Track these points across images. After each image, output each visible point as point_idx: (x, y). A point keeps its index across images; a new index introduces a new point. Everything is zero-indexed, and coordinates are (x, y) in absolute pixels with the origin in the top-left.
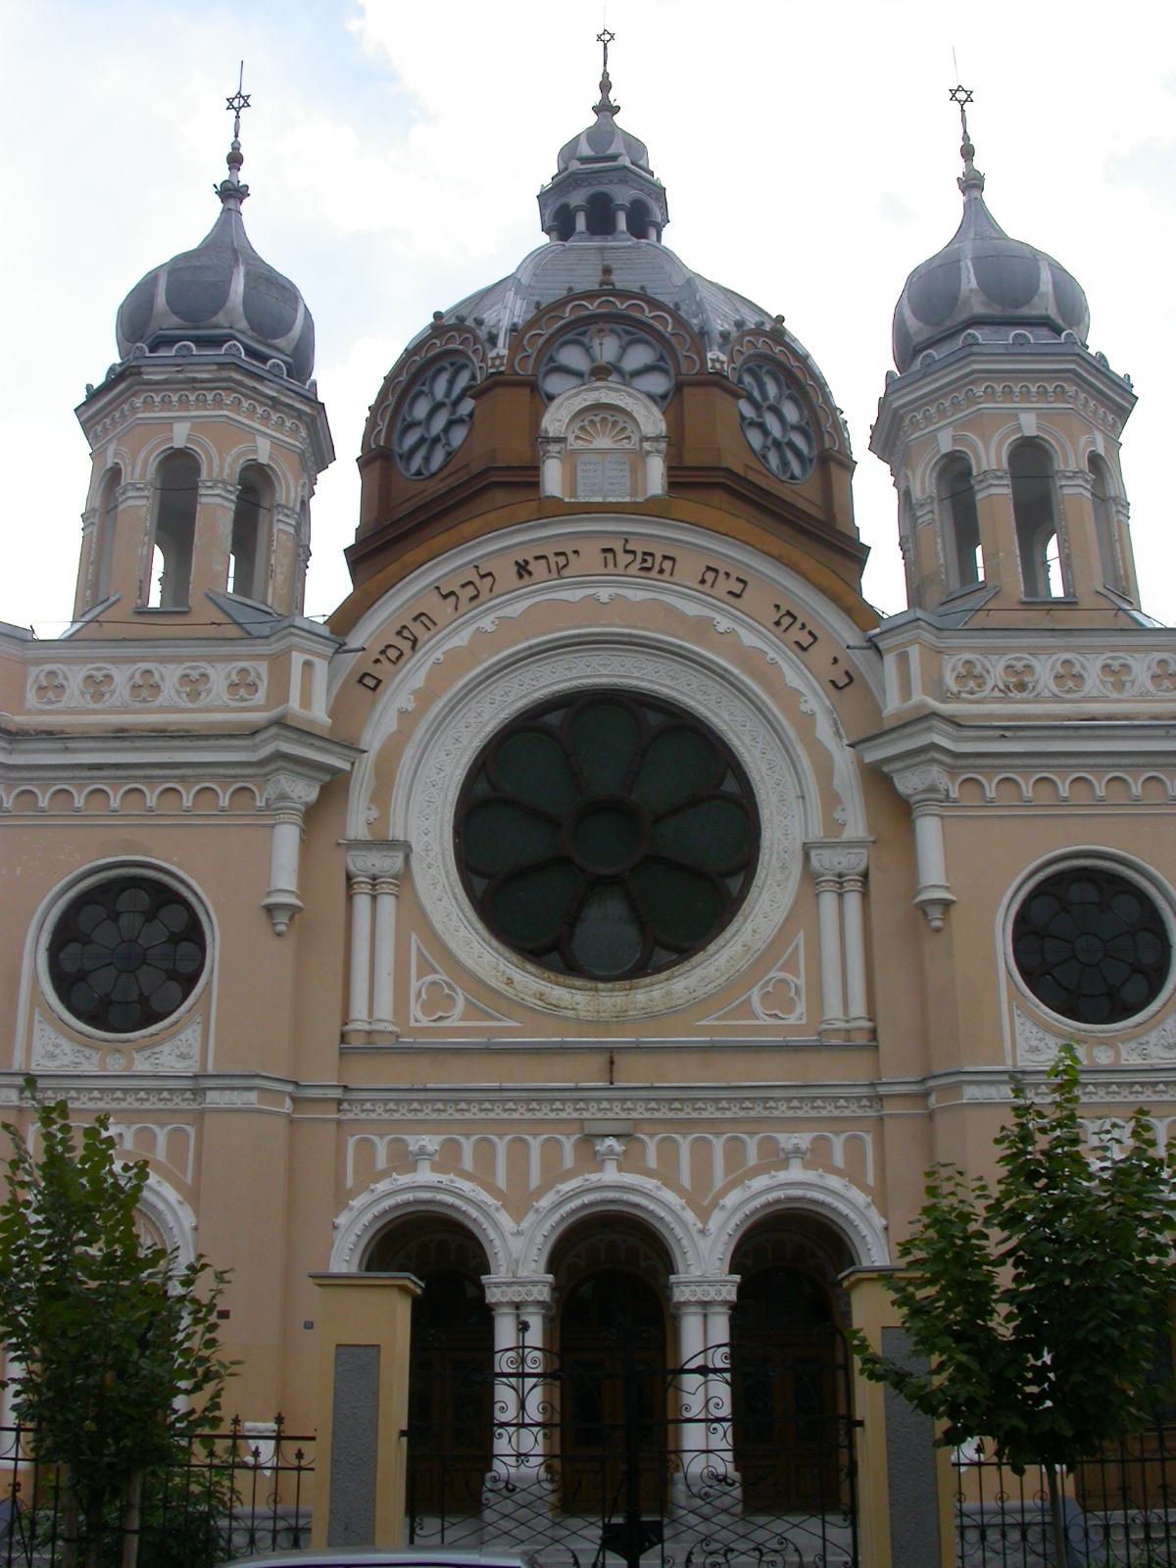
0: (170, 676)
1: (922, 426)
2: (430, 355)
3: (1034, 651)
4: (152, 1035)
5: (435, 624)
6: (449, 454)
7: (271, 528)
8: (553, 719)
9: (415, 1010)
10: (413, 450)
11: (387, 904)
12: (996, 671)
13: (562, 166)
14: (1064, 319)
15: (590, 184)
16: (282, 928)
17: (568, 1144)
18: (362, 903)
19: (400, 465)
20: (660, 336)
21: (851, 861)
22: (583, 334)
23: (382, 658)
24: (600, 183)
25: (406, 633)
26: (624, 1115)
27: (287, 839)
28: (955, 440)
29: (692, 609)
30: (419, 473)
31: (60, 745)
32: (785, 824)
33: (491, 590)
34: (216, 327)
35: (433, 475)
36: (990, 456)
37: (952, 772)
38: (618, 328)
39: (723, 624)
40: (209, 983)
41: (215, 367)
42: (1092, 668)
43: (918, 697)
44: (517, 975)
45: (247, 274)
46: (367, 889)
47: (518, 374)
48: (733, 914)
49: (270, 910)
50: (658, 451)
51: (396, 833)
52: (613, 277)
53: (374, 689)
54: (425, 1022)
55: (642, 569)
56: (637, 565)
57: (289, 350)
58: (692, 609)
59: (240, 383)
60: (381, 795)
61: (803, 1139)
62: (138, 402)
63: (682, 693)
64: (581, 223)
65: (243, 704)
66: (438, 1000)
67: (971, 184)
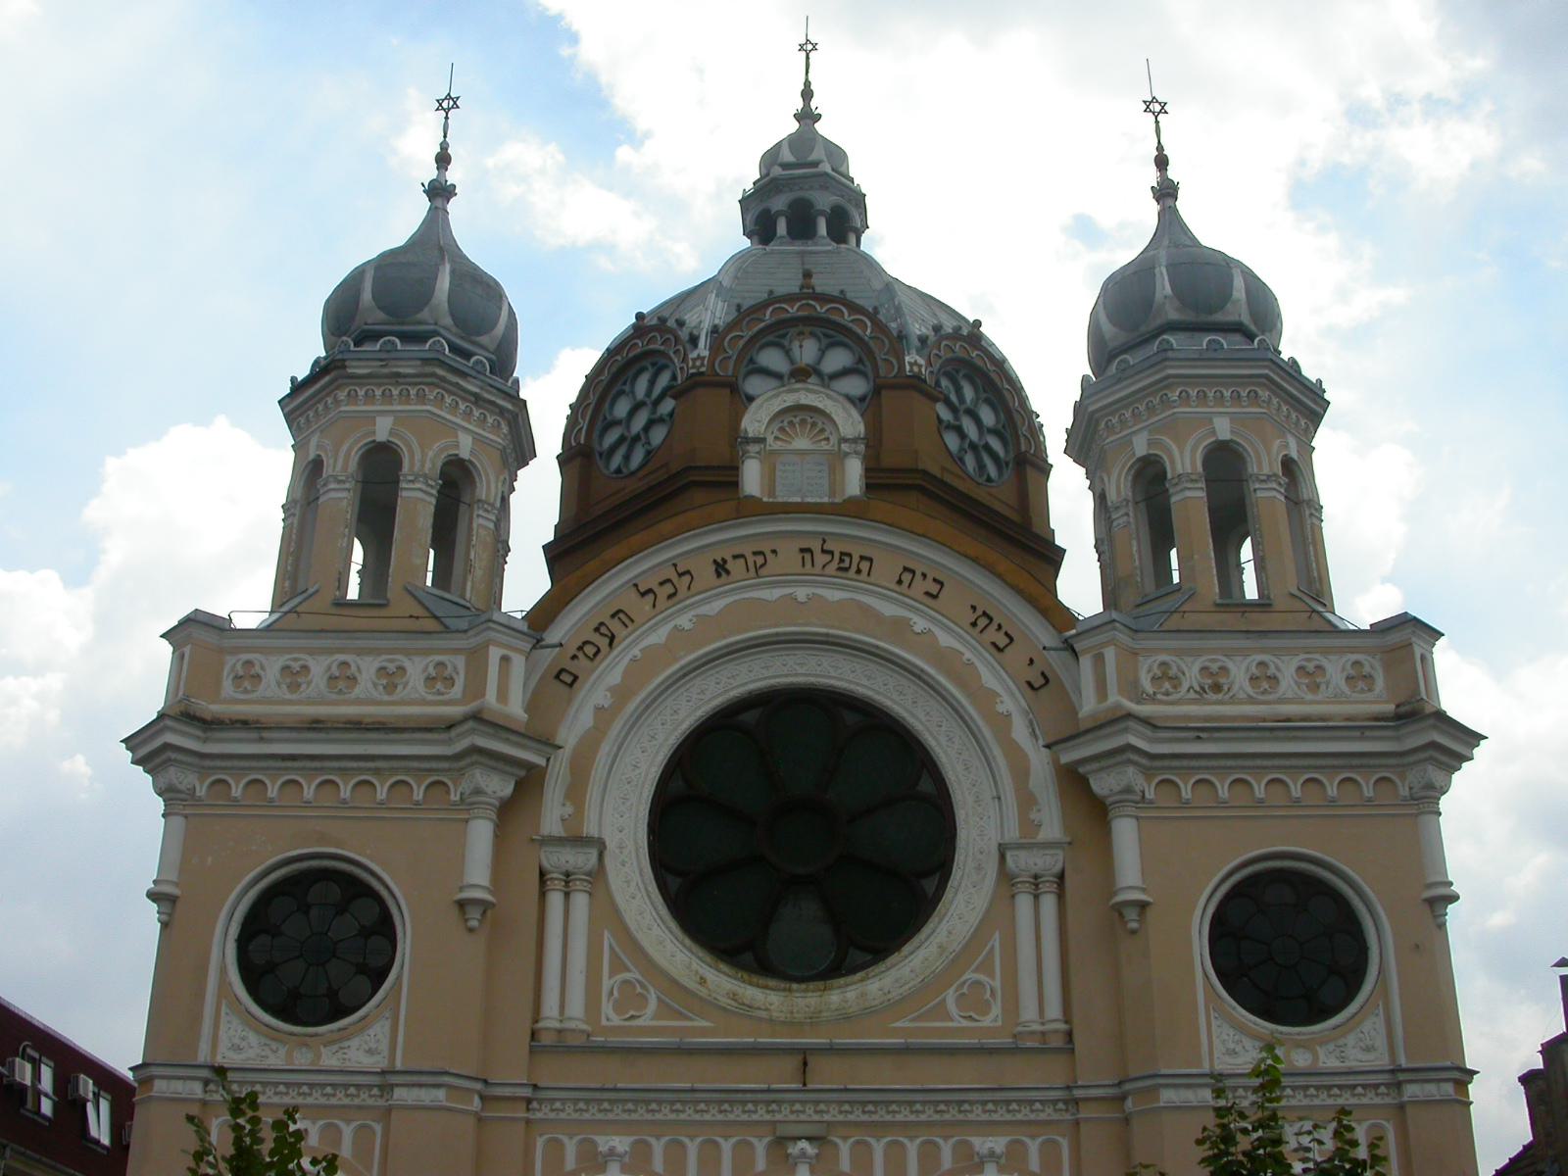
0: (367, 668)
1: (1117, 430)
2: (630, 355)
3: (1229, 653)
4: (340, 1030)
5: (632, 621)
6: (648, 453)
7: (471, 523)
8: (850, 718)
9: (607, 1008)
10: (613, 449)
11: (580, 901)
12: (1192, 673)
13: (764, 172)
14: (1256, 324)
15: (791, 190)
16: (474, 923)
17: (760, 1147)
18: (555, 900)
19: (601, 463)
20: (859, 340)
21: (1047, 862)
22: (784, 336)
23: (580, 655)
24: (801, 189)
25: (603, 630)
26: (816, 1118)
27: (481, 833)
28: (1150, 443)
29: (889, 610)
30: (618, 471)
31: (254, 735)
32: (981, 824)
33: (689, 588)
34: (420, 323)
35: (633, 473)
36: (1185, 460)
37: (1148, 774)
38: (818, 331)
39: (920, 624)
40: (399, 977)
41: (419, 363)
42: (1287, 669)
43: (1114, 697)
44: (711, 975)
45: (453, 272)
46: (560, 885)
47: (718, 375)
48: (928, 916)
49: (462, 905)
50: (856, 453)
51: (591, 829)
52: (814, 281)
53: (571, 685)
54: (616, 1021)
55: (840, 569)
56: (835, 564)
57: (492, 347)
58: (889, 610)
59: (443, 379)
60: (576, 792)
61: (998, 1143)
62: (342, 395)
63: (878, 693)
64: (782, 227)
65: (440, 698)
66: (629, 999)
67: (1166, 192)
